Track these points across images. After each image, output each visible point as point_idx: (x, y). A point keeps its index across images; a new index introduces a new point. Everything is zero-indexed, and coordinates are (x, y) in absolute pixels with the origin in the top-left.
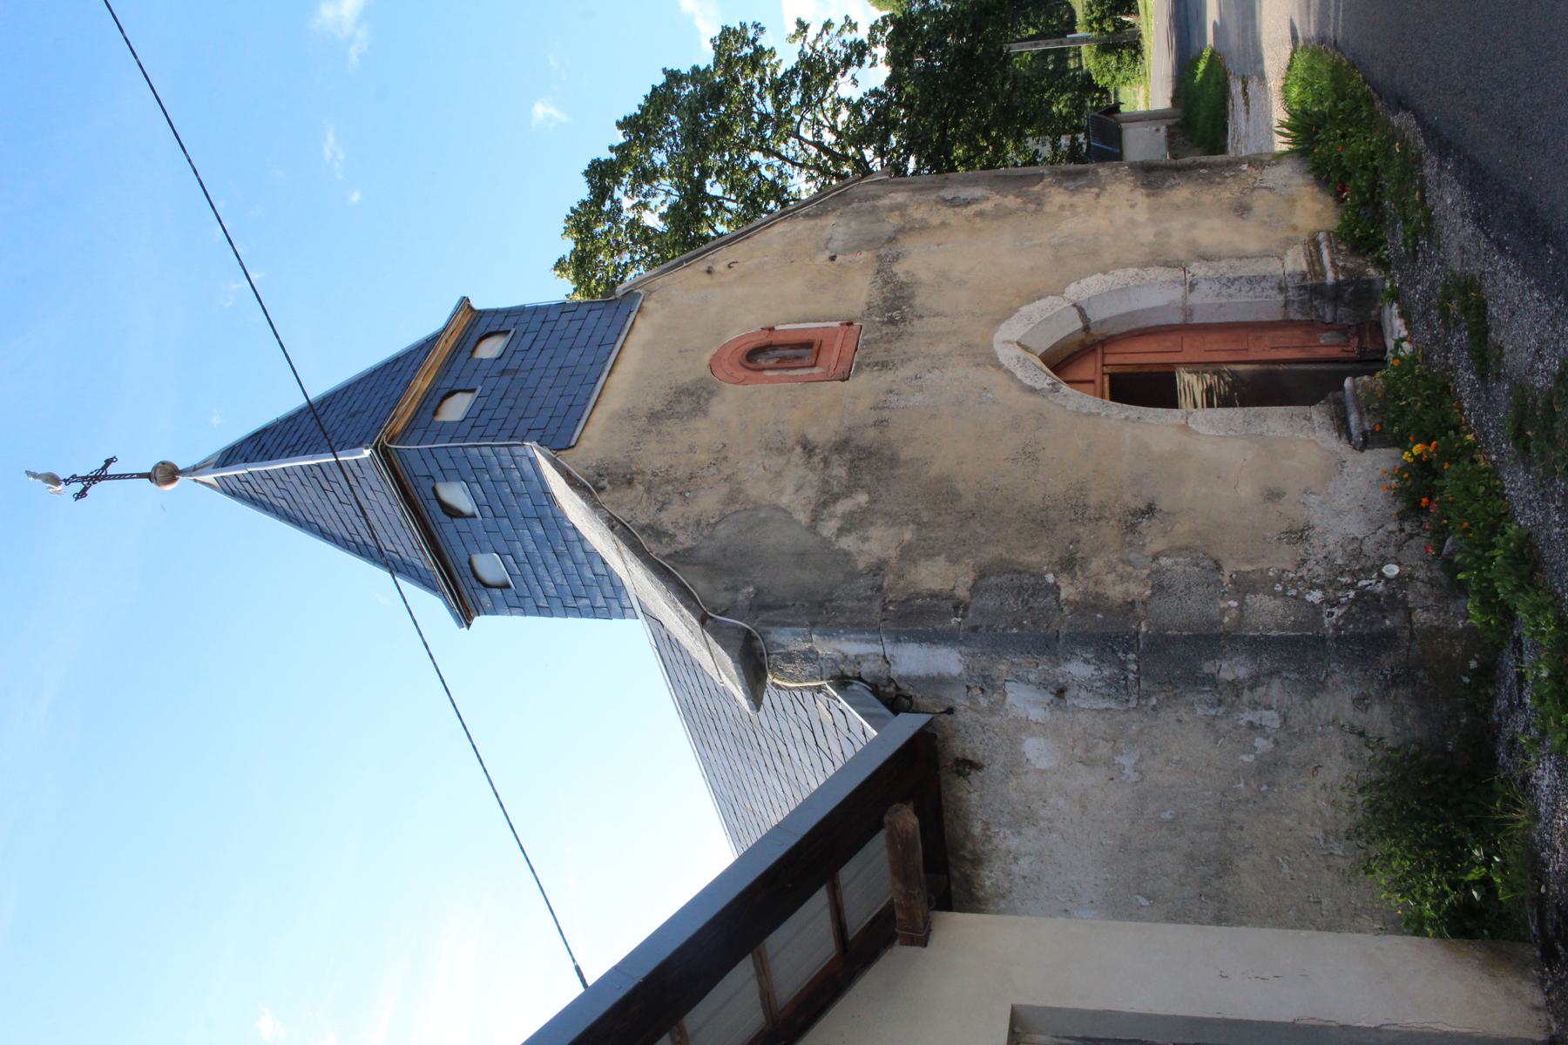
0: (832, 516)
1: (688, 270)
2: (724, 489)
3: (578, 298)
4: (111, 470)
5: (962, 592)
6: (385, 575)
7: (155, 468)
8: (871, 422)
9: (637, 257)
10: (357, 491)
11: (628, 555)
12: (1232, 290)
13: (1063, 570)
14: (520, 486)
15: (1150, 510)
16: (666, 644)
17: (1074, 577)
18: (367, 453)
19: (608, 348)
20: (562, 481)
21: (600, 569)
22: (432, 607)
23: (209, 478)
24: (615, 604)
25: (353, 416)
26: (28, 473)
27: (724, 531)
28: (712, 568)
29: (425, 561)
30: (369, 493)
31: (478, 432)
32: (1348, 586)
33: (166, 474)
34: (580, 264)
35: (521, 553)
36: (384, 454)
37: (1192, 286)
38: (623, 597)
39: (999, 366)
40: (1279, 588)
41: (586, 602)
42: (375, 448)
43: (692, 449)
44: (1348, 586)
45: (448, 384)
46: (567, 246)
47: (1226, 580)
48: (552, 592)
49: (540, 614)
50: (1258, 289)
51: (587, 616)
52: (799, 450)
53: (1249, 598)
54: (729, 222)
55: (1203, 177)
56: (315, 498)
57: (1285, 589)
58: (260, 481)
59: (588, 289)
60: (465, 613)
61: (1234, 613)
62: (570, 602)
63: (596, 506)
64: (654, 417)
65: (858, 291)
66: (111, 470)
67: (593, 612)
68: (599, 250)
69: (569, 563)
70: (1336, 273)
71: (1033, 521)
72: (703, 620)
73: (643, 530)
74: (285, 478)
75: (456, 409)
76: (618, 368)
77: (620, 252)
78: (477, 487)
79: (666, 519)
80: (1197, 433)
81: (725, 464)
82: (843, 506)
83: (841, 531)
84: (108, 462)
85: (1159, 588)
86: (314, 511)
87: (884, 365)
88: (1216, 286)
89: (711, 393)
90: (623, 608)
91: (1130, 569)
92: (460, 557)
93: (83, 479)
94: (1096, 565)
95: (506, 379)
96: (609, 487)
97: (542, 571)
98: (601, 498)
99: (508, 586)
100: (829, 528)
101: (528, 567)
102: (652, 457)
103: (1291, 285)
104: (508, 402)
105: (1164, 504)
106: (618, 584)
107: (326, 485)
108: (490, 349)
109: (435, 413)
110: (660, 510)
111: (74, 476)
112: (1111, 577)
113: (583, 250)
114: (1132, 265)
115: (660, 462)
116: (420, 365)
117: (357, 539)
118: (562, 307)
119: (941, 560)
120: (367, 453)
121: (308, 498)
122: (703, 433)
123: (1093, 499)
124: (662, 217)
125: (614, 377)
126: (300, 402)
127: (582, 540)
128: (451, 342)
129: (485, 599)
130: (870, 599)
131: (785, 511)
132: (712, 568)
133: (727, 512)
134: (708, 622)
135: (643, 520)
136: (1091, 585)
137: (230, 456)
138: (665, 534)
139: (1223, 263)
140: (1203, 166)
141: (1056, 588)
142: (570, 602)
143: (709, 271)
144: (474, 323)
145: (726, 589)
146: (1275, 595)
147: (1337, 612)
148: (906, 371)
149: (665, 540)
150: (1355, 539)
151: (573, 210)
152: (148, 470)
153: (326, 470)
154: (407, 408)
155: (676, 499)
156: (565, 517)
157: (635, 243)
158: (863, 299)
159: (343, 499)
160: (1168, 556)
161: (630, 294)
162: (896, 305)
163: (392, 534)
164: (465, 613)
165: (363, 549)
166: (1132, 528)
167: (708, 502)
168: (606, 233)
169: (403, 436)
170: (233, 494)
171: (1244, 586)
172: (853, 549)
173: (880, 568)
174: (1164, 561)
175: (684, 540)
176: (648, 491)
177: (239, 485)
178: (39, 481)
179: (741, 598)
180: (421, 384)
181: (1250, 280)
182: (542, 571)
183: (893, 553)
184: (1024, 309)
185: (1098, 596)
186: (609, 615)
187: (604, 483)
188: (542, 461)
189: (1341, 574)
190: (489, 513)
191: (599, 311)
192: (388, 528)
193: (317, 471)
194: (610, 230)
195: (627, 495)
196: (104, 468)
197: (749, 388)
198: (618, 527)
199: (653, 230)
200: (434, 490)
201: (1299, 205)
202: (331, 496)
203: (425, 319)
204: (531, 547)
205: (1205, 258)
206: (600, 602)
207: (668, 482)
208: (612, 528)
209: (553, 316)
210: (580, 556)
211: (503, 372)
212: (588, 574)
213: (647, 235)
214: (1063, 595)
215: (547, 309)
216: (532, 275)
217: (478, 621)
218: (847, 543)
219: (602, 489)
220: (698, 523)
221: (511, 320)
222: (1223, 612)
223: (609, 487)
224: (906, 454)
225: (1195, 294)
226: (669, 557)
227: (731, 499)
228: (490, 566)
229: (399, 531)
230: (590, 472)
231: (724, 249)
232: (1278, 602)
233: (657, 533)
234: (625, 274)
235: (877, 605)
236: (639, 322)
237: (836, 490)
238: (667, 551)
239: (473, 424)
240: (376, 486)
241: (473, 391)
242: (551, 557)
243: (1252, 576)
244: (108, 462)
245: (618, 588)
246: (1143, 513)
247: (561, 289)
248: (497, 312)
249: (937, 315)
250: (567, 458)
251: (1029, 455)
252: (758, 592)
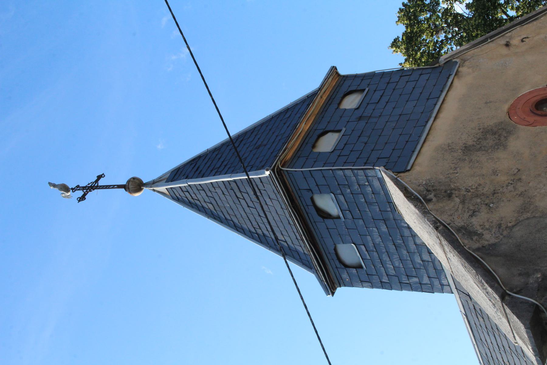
1: (491, 45)
2: (519, 202)
3: (407, 66)
4: (101, 182)
6: (279, 258)
7: (129, 182)
9: (450, 36)
10: (261, 198)
11: (448, 248)
14: (371, 197)
16: (472, 312)
18: (267, 173)
19: (434, 101)
20: (401, 194)
21: (426, 257)
22: (309, 280)
23: (163, 189)
24: (436, 283)
25: (258, 148)
26: (50, 184)
27: (519, 232)
28: (510, 259)
29: (304, 247)
30: (268, 201)
31: (344, 159)
33: (135, 185)
34: (409, 42)
35: (371, 244)
36: (279, 174)
38: (443, 277)
41: (416, 280)
42: (273, 170)
43: (495, 172)
45: (322, 127)
46: (400, 30)
48: (392, 272)
49: (383, 287)
51: (416, 290)
54: (518, 9)
56: (231, 203)
58: (196, 191)
59: (416, 60)
60: (331, 285)
62: (404, 279)
63: (425, 213)
64: (467, 149)
66: (101, 182)
67: (420, 287)
68: (422, 32)
69: (405, 252)
72: (503, 297)
73: (459, 230)
74: (212, 190)
75: (327, 143)
76: (441, 115)
77: (437, 33)
78: (341, 198)
79: (476, 222)
81: (519, 184)
84: (99, 177)
86: (230, 212)
89: (510, 133)
90: (442, 285)
92: (334, 244)
93: (83, 188)
95: (362, 123)
96: (434, 199)
97: (385, 257)
98: (429, 207)
99: (361, 267)
101: (375, 254)
102: (467, 178)
104: (364, 139)
106: (439, 268)
107: (239, 195)
108: (351, 102)
109: (314, 146)
110: (471, 216)
111: (78, 186)
113: (412, 32)
115: (471, 182)
116: (303, 113)
117: (259, 231)
118: (401, 72)
120: (267, 173)
121: (227, 203)
122: (504, 161)
124: (468, 6)
125: (438, 121)
126: (224, 137)
127: (414, 236)
128: (324, 98)
129: (345, 276)
132: (510, 259)
133: (521, 219)
134: (507, 298)
135: (459, 223)
137: (176, 174)
138: (475, 233)
142: (404, 279)
143: (507, 45)
144: (339, 84)
145: (520, 275)
149: (475, 238)
151: (404, 5)
152: (124, 183)
153: (240, 184)
154: (294, 143)
155: (484, 208)
156: (402, 220)
157: (449, 26)
159: (251, 204)
161: (450, 63)
163: (282, 229)
164: (331, 285)
165: (263, 239)
167: (507, 211)
168: (428, 20)
169: (291, 163)
170: (178, 200)
175: (489, 238)
176: (463, 202)
177: (182, 194)
178: (56, 189)
179: (531, 281)
180: (304, 126)
182: (385, 257)
186: (431, 290)
187: (431, 196)
188: (387, 180)
190: (349, 216)
191: (426, 73)
192: (280, 224)
193: (234, 185)
194: (430, 18)
195: (448, 205)
196: (97, 181)
197: (538, 129)
198: (441, 228)
199: (461, 15)
200: (312, 199)
202: (243, 202)
203: (307, 81)
204: (378, 240)
206: (426, 280)
207: (477, 196)
208: (437, 228)
209: (395, 79)
210: (413, 247)
211: (360, 118)
212: (418, 260)
213: (457, 19)
215: (383, 75)
216: (375, 50)
217: (340, 291)
219: (430, 201)
220: (500, 226)
221: (367, 82)
223: (434, 199)
226: (478, 250)
227: (524, 209)
228: (349, 253)
229: (288, 227)
230: (421, 188)
231: (518, 28)
233: (469, 232)
234: (441, 48)
236: (456, 82)
238: (476, 246)
239: (339, 155)
240: (273, 196)
241: (339, 131)
242: (392, 248)
244: (99, 177)
245: (439, 271)
247: (395, 61)
248: (356, 76)
250: (404, 178)
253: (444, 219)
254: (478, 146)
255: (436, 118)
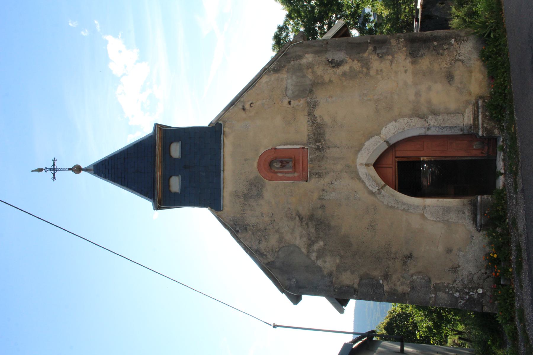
0: (313, 251)
2: (277, 236)
5: (356, 286)
8: (319, 206)
12: (444, 130)
13: (385, 279)
15: (410, 256)
17: (388, 282)
26: (32, 171)
32: (467, 293)
33: (77, 169)
37: (428, 129)
39: (360, 179)
40: (447, 290)
44: (467, 293)
47: (432, 286)
50: (453, 130)
52: (297, 218)
53: (438, 293)
55: (435, 49)
57: (449, 291)
61: (433, 299)
64: (246, 197)
65: (302, 130)
70: (483, 131)
71: (375, 257)
80: (427, 219)
82: (316, 247)
83: (318, 258)
85: (413, 288)
87: (319, 175)
88: (437, 129)
91: (404, 280)
94: (394, 277)
96: (240, 231)
98: (239, 236)
100: (313, 256)
103: (465, 129)
105: (414, 254)
110: (259, 243)
112: (399, 283)
114: (405, 116)
119: (348, 272)
123: (393, 250)
130: (330, 286)
131: (298, 247)
136: (393, 286)
139: (441, 117)
140: (435, 38)
141: (382, 286)
144: (165, 134)
146: (445, 292)
147: (463, 302)
148: (327, 180)
150: (471, 274)
158: (306, 133)
160: (415, 275)
162: (318, 134)
166: (405, 263)
171: (437, 289)
172: (321, 266)
173: (331, 275)
174: (415, 277)
176: (253, 234)
181: (450, 128)
183: (334, 269)
184: (367, 143)
185: (395, 290)
187: (238, 229)
189: (466, 288)
201: (473, 74)
205: (435, 113)
214: (385, 289)
218: (320, 263)
219: (238, 231)
222: (430, 298)
224: (333, 223)
225: (429, 131)
230: (232, 223)
232: (446, 295)
235: (332, 289)
237: (313, 239)
243: (440, 285)
246: (409, 257)
249: (335, 146)
251: (372, 226)
252: (297, 282)
253: (247, 243)
254: (250, 195)
255: (223, 171)
